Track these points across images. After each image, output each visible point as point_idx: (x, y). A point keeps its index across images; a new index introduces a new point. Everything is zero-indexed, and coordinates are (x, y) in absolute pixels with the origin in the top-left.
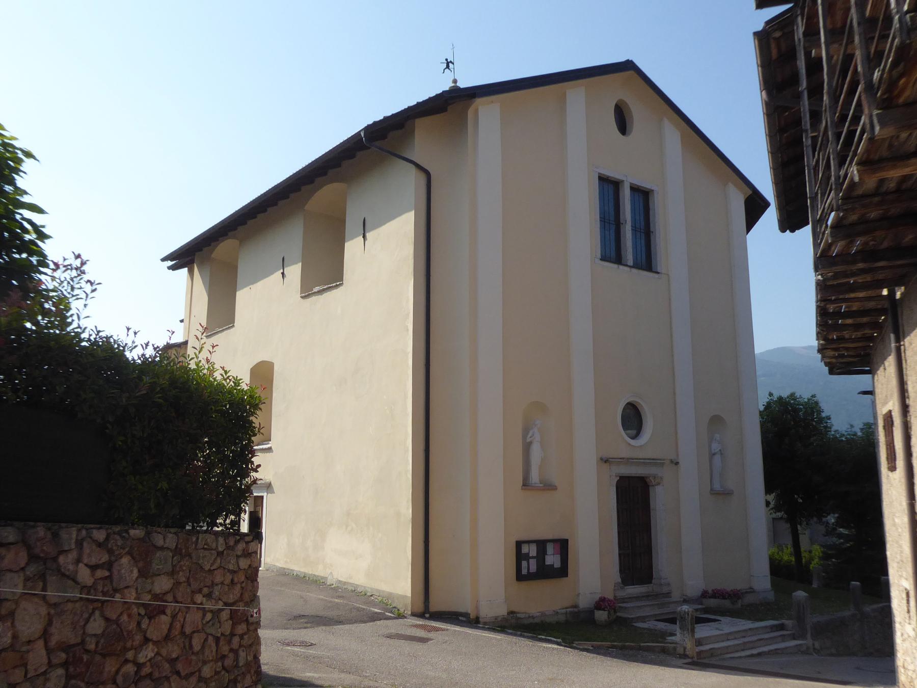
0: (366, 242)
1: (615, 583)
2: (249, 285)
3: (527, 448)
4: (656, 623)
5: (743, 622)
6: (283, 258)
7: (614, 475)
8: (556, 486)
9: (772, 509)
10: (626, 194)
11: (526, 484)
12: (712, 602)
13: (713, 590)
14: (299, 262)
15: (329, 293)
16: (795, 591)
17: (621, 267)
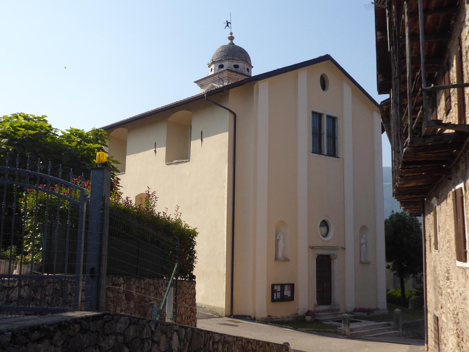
0: (203, 143)
1: (314, 304)
2: (135, 153)
3: (277, 241)
4: (332, 322)
5: (372, 322)
6: (155, 143)
7: (315, 254)
8: (289, 259)
9: (391, 269)
10: (325, 119)
11: (276, 259)
12: (358, 314)
13: (359, 308)
14: (165, 146)
15: (182, 164)
16: (396, 308)
17: (321, 156)
